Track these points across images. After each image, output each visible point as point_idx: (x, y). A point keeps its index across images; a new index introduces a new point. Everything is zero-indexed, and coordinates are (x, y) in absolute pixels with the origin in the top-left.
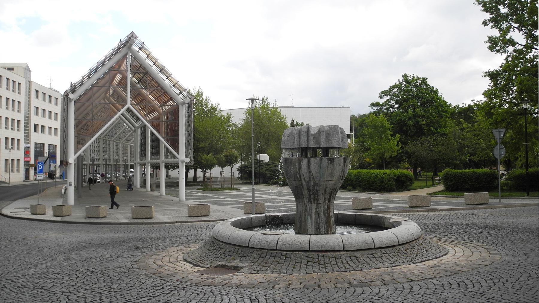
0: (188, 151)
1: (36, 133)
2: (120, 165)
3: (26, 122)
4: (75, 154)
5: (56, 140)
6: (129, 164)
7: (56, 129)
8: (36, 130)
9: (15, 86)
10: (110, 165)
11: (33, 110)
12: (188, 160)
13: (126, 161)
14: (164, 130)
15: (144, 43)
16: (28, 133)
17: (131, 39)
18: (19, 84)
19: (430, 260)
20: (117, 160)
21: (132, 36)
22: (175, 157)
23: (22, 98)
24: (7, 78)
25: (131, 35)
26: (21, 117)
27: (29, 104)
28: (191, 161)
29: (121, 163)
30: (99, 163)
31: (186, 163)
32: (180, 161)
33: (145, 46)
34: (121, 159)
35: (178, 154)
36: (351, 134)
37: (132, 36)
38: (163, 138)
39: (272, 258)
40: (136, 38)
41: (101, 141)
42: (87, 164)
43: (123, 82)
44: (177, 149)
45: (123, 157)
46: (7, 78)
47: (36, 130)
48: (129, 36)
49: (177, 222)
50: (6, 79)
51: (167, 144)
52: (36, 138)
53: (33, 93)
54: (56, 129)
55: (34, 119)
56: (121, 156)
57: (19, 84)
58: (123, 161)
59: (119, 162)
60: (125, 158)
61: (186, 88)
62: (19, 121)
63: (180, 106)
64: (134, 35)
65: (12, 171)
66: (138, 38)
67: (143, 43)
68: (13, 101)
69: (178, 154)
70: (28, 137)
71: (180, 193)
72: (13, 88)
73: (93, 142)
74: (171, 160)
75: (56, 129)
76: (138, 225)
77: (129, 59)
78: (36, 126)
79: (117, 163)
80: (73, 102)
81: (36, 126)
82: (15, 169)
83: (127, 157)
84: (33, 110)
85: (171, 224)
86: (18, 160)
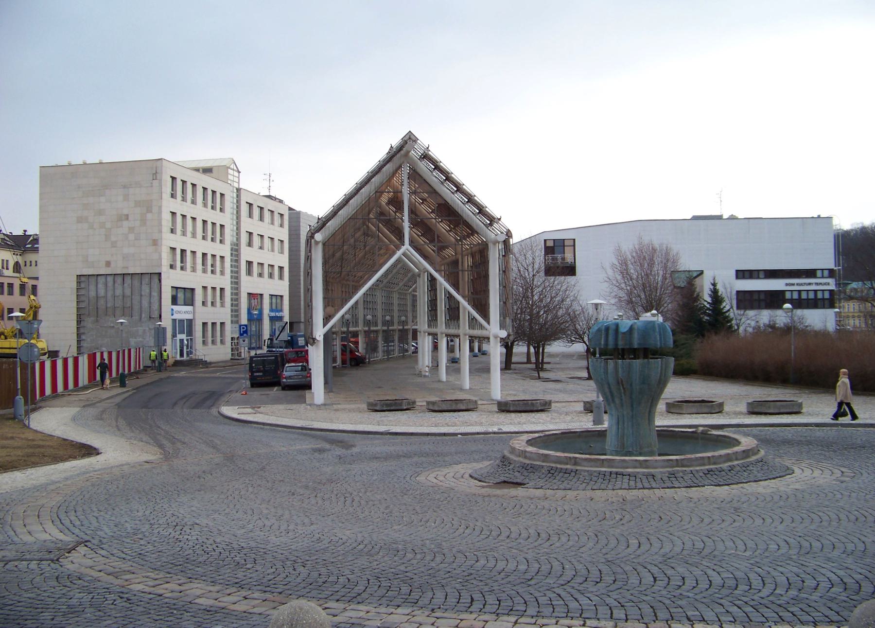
0: (504, 318)
1: (249, 278)
2: (393, 330)
3: (233, 263)
4: (324, 325)
5: (282, 287)
6: (409, 329)
7: (281, 268)
8: (249, 272)
9: (215, 199)
10: (377, 331)
11: (244, 238)
12: (504, 334)
13: (404, 323)
14: (467, 279)
15: (429, 148)
16: (237, 278)
17: (410, 139)
18: (222, 195)
19: (744, 483)
20: (390, 323)
21: (410, 138)
22: (482, 327)
23: (226, 219)
24: (203, 187)
25: (407, 137)
26: (225, 250)
27: (238, 229)
28: (509, 335)
29: (396, 327)
30: (357, 329)
31: (501, 339)
32: (491, 333)
33: (430, 153)
34: (396, 320)
35: (489, 323)
36: (835, 268)
37: (410, 138)
38: (463, 297)
39: (584, 485)
40: (415, 140)
41: (361, 306)
42: (338, 332)
43: (396, 202)
44: (485, 315)
45: (399, 317)
46: (203, 187)
47: (249, 272)
48: (405, 139)
49: (478, 433)
50: (202, 189)
51: (470, 308)
52: (249, 284)
53: (244, 208)
54: (281, 268)
55: (247, 254)
56: (396, 314)
57: (222, 195)
58: (399, 323)
59: (393, 325)
60: (403, 318)
61: (499, 218)
62: (222, 258)
63: (491, 246)
64: (412, 137)
65: (213, 342)
66: (418, 141)
67: (428, 148)
68: (214, 224)
69: (489, 323)
70: (237, 283)
71: (492, 381)
72: (213, 202)
73: (349, 309)
74: (477, 332)
75: (281, 268)
76: (422, 437)
77: (406, 170)
78: (250, 263)
79: (388, 328)
80: (320, 246)
81: (250, 263)
82: (218, 339)
83: (406, 317)
84: (244, 238)
85: (470, 436)
86: (222, 324)
